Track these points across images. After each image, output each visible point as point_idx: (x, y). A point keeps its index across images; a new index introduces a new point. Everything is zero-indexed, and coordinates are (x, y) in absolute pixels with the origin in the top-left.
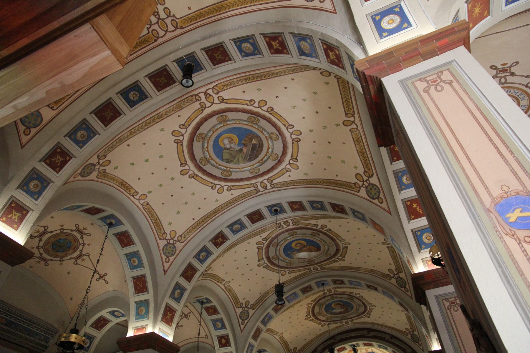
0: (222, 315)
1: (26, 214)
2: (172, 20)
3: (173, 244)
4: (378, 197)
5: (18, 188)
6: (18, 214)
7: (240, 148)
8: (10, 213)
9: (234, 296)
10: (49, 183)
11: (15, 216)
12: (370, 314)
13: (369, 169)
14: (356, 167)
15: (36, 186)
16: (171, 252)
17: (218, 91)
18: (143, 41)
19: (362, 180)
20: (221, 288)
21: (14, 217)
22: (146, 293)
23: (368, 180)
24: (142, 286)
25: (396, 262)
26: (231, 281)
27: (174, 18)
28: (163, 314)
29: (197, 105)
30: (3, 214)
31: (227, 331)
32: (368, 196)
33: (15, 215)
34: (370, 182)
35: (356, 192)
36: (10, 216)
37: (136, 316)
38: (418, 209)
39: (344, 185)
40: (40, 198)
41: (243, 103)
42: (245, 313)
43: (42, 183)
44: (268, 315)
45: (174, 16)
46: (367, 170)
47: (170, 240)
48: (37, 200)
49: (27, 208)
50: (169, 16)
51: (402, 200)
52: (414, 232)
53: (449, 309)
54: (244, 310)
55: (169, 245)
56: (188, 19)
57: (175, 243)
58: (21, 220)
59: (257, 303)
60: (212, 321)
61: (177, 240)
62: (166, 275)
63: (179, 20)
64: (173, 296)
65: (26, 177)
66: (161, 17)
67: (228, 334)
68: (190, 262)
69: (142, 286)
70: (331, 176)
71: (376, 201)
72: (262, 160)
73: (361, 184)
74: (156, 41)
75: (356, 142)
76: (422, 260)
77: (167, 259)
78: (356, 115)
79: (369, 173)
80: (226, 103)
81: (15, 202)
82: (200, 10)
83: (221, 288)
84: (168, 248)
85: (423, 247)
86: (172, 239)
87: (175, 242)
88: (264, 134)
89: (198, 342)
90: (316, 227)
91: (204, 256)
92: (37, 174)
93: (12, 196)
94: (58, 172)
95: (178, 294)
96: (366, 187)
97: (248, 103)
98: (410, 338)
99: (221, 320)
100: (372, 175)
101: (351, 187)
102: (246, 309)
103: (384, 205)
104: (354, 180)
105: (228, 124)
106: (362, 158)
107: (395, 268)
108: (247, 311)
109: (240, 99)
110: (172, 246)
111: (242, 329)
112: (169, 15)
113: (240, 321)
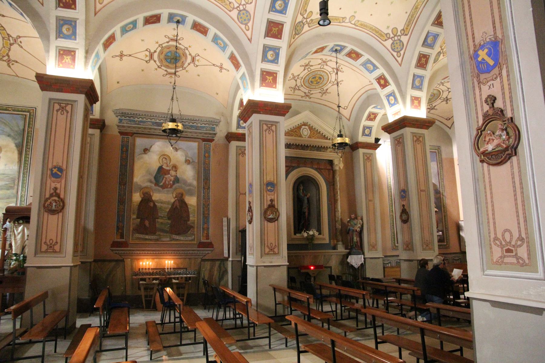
0: (366, 56)
1: (75, 54)
3: (244, 9)
5: (56, 39)
6: (69, 57)
8: (63, 59)
9: (373, 30)
10: (76, 22)
11: (68, 59)
15: (68, 29)
16: (247, 19)
19: (395, 34)
20: (349, 27)
21: (67, 61)
26: (355, 15)
28: (260, 80)
30: (58, 62)
31: (381, 71)
33: (67, 59)
36: (64, 61)
40: (77, 37)
42: (397, 43)
43: (71, 25)
44: (430, 35)
47: (238, 7)
48: (76, 40)
49: (73, 50)
54: (395, 40)
55: (241, 13)
57: (246, 7)
58: (74, 59)
59: (408, 26)
60: (363, 66)
61: (245, 3)
62: (252, 42)
64: (266, 60)
65: (57, 26)
67: (383, 73)
68: (268, 19)
77: (247, 27)
78: (354, 26)
81: (62, 50)
83: (349, 27)
84: (242, 15)
86: (240, 4)
87: (244, 6)
91: (281, 6)
92: (63, 20)
93: (57, 47)
94: (75, 9)
95: (272, 55)
99: (369, 62)
102: (396, 38)
108: (399, 40)
110: (244, 12)
111: (400, 61)
113: (395, 54)
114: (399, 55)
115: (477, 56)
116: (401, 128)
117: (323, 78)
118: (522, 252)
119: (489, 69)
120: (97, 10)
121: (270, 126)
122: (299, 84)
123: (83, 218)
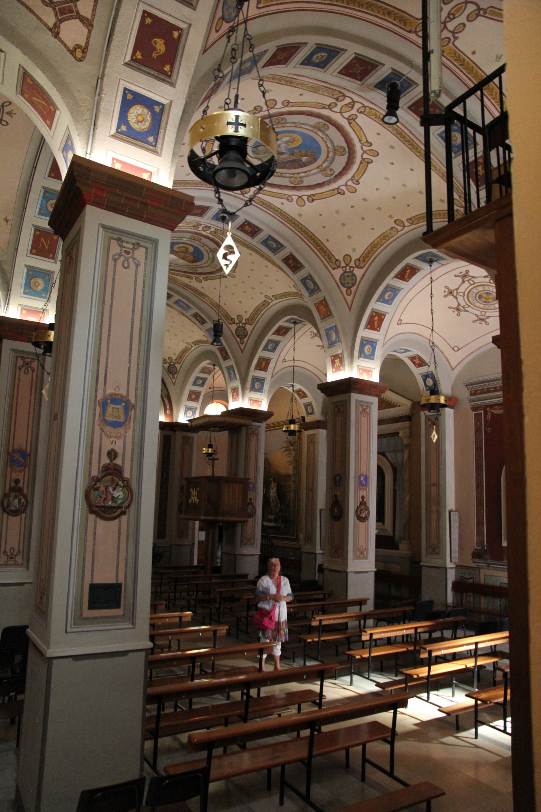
2: (449, 38)
4: (349, 288)
7: (284, 151)
12: (358, 181)
13: (364, 261)
14: (354, 250)
17: (364, 112)
18: (404, 19)
19: (348, 263)
22: (52, 261)
23: (354, 268)
24: (47, 247)
25: (256, 314)
27: (452, 40)
29: (328, 101)
32: (340, 279)
34: (353, 270)
35: (331, 267)
37: (25, 288)
38: (376, 322)
39: (325, 252)
41: (361, 136)
45: (456, 38)
46: (361, 259)
50: (453, 33)
51: (373, 309)
52: (363, 339)
53: (361, 413)
56: (458, 56)
63: (452, 46)
66: (448, 25)
69: (47, 247)
70: (321, 236)
71: (344, 290)
72: (282, 173)
73: (343, 264)
74: (410, 32)
75: (382, 237)
76: (358, 366)
79: (360, 264)
80: (350, 124)
82: (477, 66)
85: (362, 355)
88: (324, 163)
89: (213, 391)
90: (196, 229)
96: (345, 272)
97: (364, 140)
98: (167, 368)
100: (361, 268)
101: (330, 259)
102: (241, 325)
103: (349, 299)
104: (340, 257)
105: (316, 133)
106: (369, 248)
107: (247, 317)
109: (364, 133)
112: (455, 31)
114: (349, 292)
115: (360, 478)
116: (315, 428)
117: (476, 297)
118: (365, 553)
119: (363, 486)
120: (349, 303)
121: (29, 360)
122: (462, 289)
123: (304, 524)
